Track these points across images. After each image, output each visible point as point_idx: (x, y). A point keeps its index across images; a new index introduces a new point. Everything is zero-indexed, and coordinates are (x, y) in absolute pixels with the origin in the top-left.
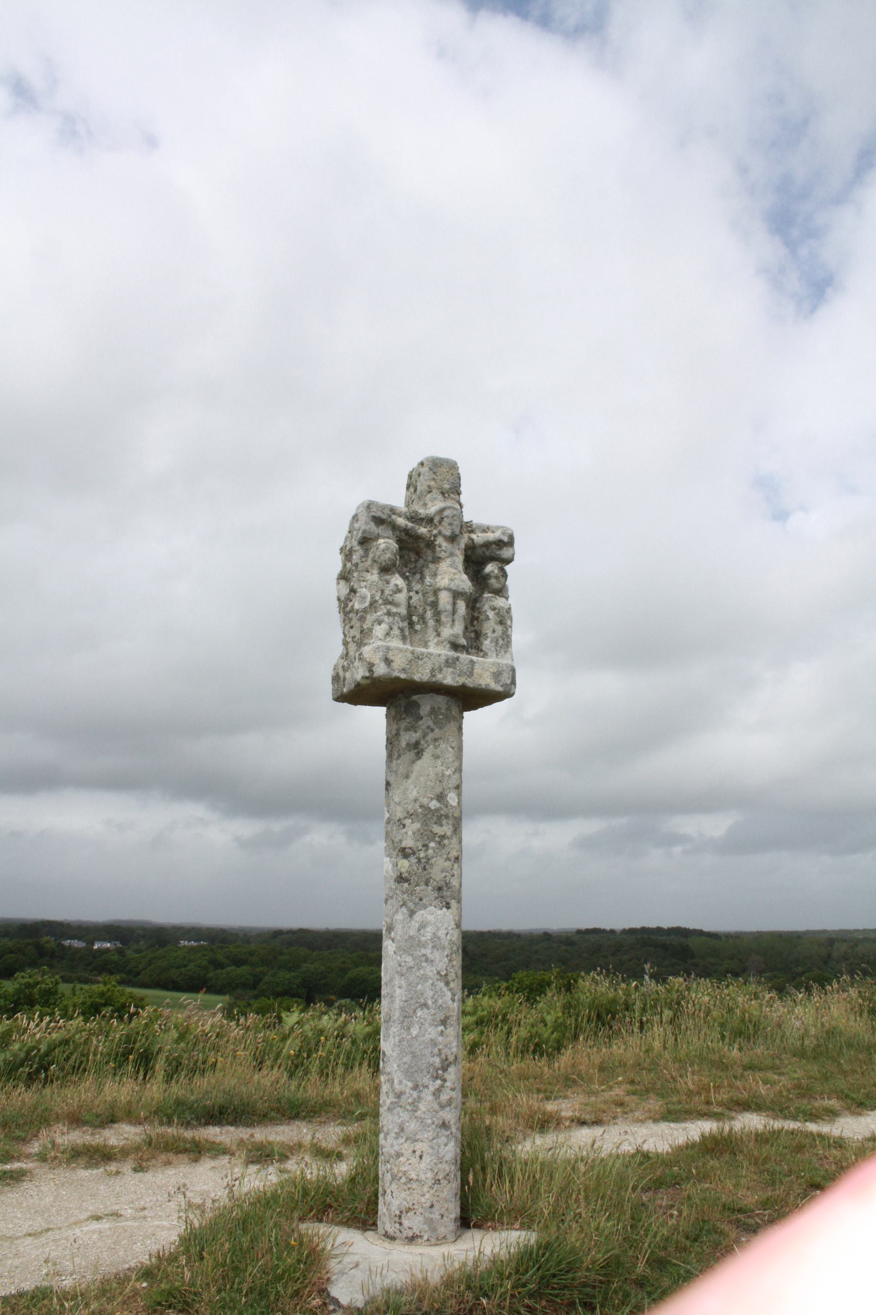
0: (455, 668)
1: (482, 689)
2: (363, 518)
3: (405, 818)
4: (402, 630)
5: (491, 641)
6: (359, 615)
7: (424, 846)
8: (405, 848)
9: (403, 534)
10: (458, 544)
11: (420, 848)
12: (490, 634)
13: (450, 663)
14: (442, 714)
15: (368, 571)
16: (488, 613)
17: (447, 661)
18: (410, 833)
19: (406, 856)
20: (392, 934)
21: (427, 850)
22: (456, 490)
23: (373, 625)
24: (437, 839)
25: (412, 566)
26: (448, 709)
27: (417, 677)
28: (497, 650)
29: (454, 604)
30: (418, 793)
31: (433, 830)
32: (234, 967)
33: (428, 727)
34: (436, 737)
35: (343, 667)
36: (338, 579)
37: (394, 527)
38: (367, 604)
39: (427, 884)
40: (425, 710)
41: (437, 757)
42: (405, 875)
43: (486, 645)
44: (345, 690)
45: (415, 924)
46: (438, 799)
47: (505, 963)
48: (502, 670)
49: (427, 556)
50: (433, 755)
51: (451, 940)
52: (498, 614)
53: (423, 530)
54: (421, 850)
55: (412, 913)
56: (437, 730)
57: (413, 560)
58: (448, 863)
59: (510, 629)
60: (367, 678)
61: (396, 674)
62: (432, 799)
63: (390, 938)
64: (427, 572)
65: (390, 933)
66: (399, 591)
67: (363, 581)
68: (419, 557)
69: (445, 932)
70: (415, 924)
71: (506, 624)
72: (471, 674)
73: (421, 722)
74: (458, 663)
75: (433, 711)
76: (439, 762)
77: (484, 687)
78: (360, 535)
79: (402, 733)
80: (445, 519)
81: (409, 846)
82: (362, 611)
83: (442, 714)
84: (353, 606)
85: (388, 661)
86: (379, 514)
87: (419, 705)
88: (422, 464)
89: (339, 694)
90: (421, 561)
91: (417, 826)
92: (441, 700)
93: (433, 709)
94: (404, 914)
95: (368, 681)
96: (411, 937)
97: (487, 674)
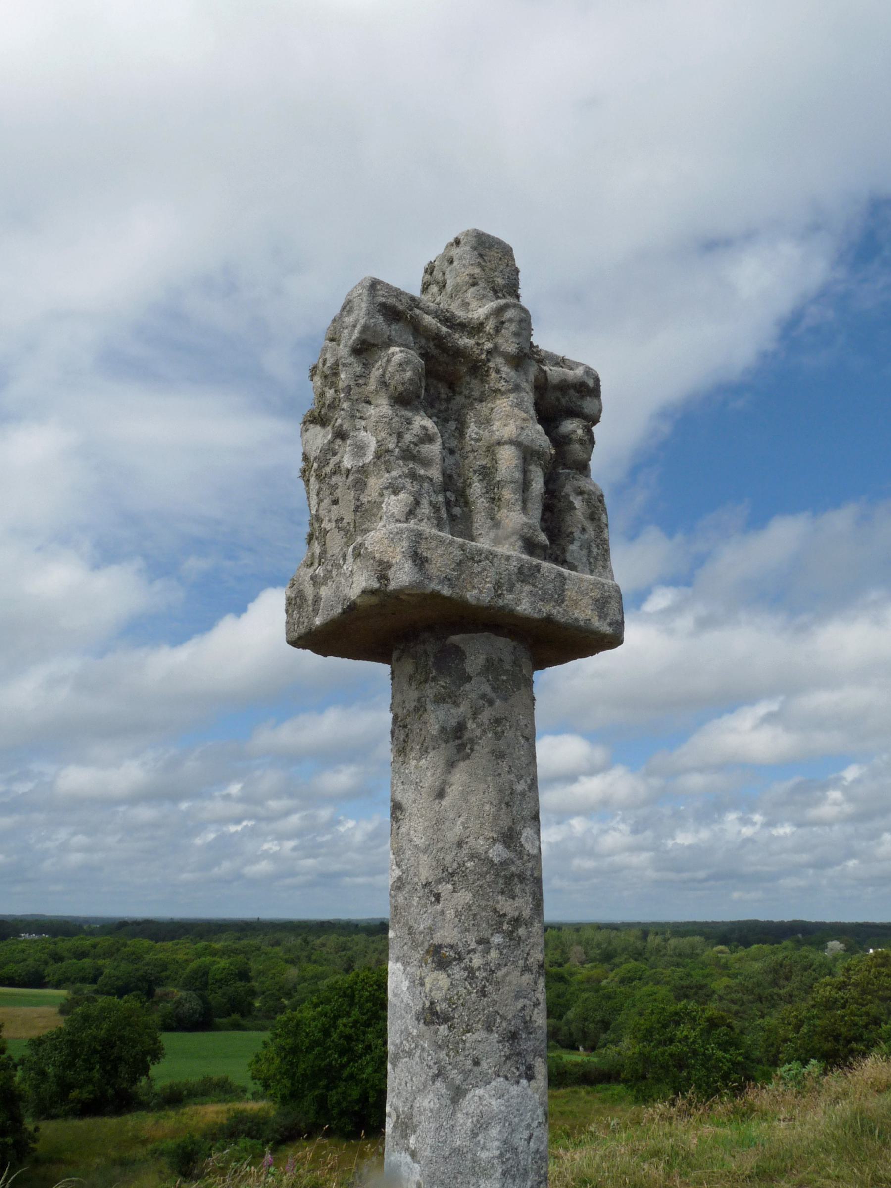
0: (534, 585)
1: (579, 629)
2: (362, 307)
3: (439, 881)
4: (435, 507)
5: (581, 548)
6: (351, 477)
7: (480, 942)
8: (440, 947)
9: (431, 344)
10: (526, 373)
11: (473, 946)
12: (577, 534)
13: (526, 575)
14: (506, 672)
15: (369, 403)
16: (571, 499)
17: (520, 570)
18: (450, 913)
19: (442, 964)
20: (412, 1140)
21: (487, 952)
22: (512, 288)
23: (381, 495)
24: (505, 926)
25: (443, 408)
26: (515, 663)
27: (470, 596)
28: (590, 563)
29: (525, 472)
30: (465, 828)
31: (499, 907)
32: (75, 961)
33: (483, 696)
34: (498, 716)
35: (313, 578)
36: (305, 423)
37: (416, 327)
38: (369, 457)
39: (489, 1029)
40: (474, 663)
41: (499, 755)
42: (442, 1007)
43: (573, 552)
44: (318, 621)
45: (464, 1121)
46: (505, 842)
47: (343, 953)
48: (610, 597)
49: (471, 390)
50: (493, 752)
51: (537, 1151)
52: (588, 502)
53: (465, 341)
54: (474, 951)
55: (458, 1094)
56: (498, 703)
57: (443, 396)
58: (527, 978)
59: (606, 530)
60: (373, 592)
61: (434, 586)
62: (494, 841)
63: (407, 1149)
64: (471, 418)
65: (405, 1136)
66: (428, 438)
67: (361, 418)
68: (454, 392)
69: (526, 1134)
70: (464, 1121)
71: (600, 519)
72: (560, 601)
73: (467, 687)
74: (538, 575)
75: (491, 667)
76: (504, 765)
77: (582, 623)
78: (356, 334)
79: (430, 707)
80: (507, 325)
81: (448, 941)
82: (358, 471)
83: (506, 672)
84: (338, 465)
85: (419, 560)
86: (391, 301)
87: (463, 653)
88: (457, 242)
89: (303, 630)
90: (459, 400)
91: (465, 897)
92: (503, 647)
93: (489, 660)
94: (440, 1097)
95: (374, 600)
96: (457, 1151)
97: (586, 600)
